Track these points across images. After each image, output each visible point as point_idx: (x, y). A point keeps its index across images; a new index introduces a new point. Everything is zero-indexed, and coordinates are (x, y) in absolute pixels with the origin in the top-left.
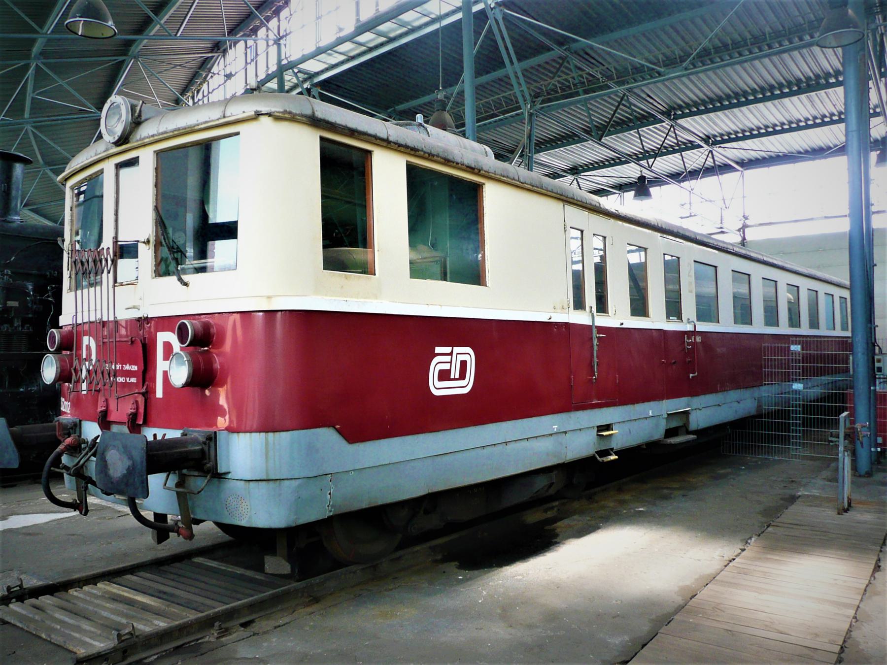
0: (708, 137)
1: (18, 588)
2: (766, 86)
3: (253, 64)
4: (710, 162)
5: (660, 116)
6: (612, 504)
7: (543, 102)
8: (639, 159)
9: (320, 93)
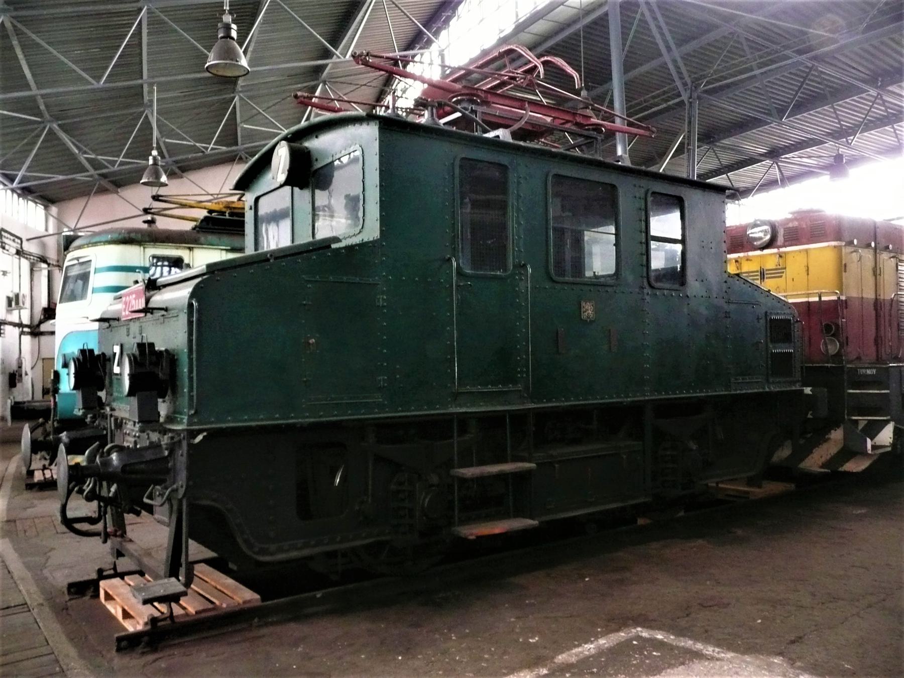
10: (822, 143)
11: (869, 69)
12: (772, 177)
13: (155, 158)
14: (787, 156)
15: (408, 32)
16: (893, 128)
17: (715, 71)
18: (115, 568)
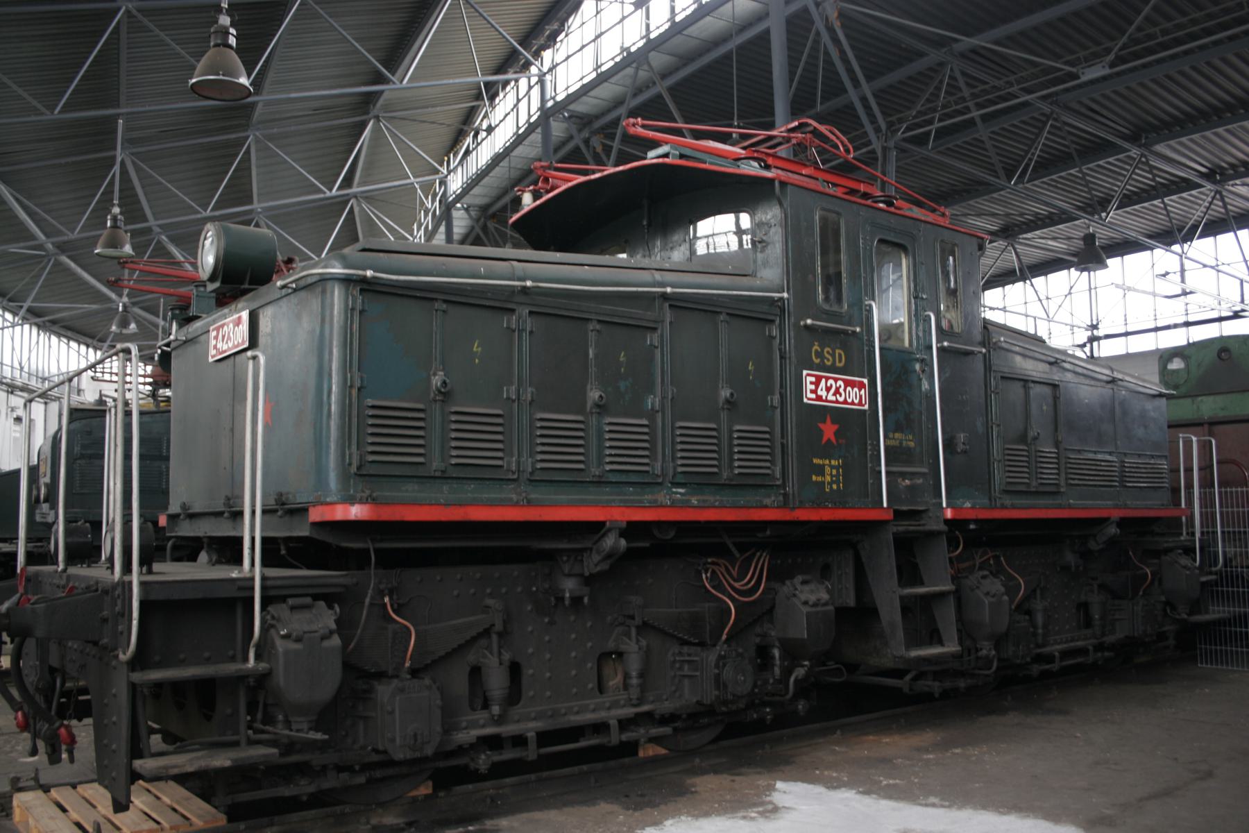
3: (526, 99)
4: (1218, 209)
5: (1119, 142)
6: (753, 815)
7: (908, 129)
10: (1072, 219)
11: (1130, 123)
12: (1008, 265)
13: (115, 219)
14: (1029, 235)
15: (498, 53)
16: (1163, 202)
17: (919, 112)
18: (36, 779)
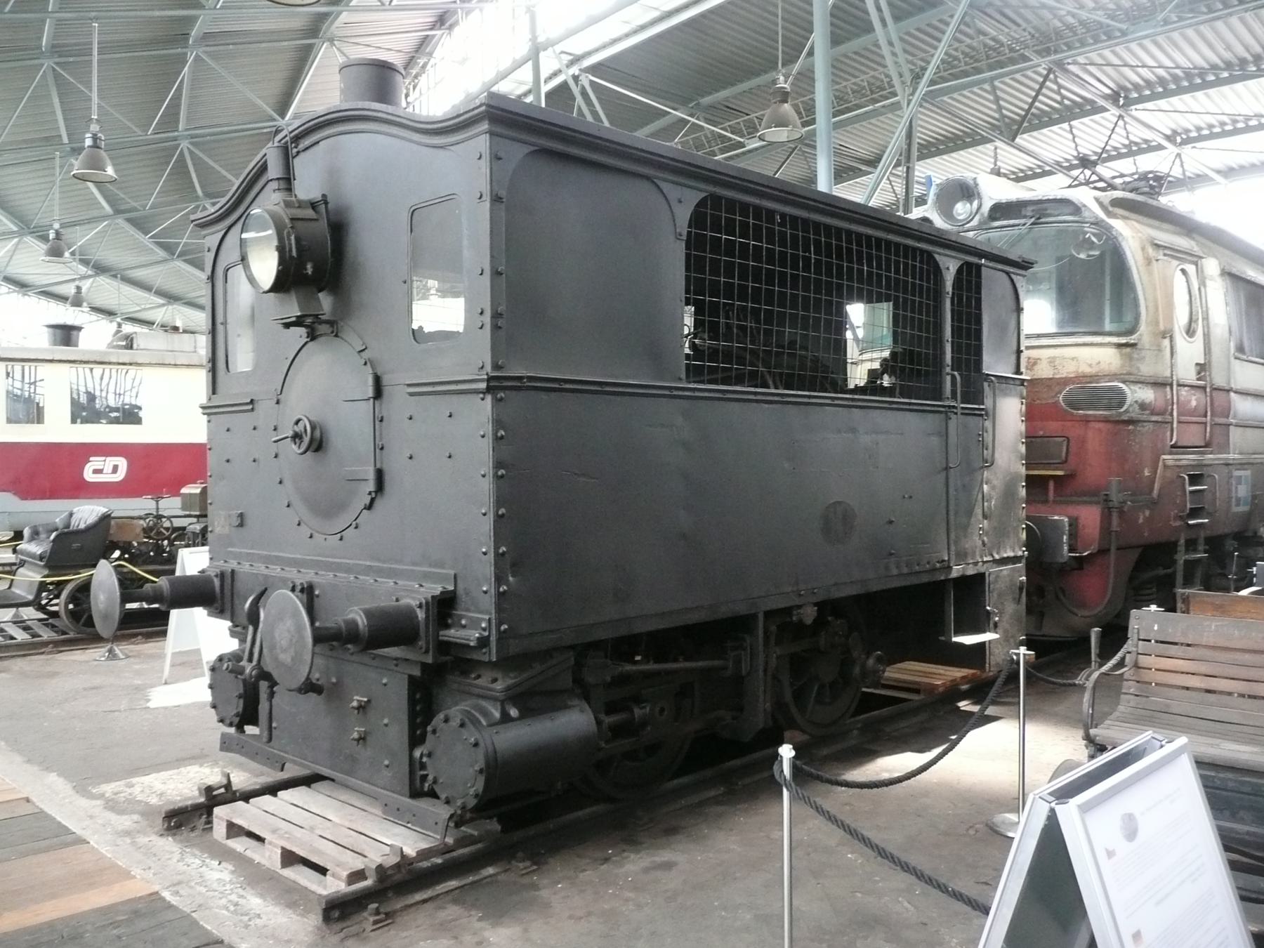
0: (1175, 132)
1: (222, 790)
2: (1235, 61)
8: (1071, 167)
9: (591, 81)
